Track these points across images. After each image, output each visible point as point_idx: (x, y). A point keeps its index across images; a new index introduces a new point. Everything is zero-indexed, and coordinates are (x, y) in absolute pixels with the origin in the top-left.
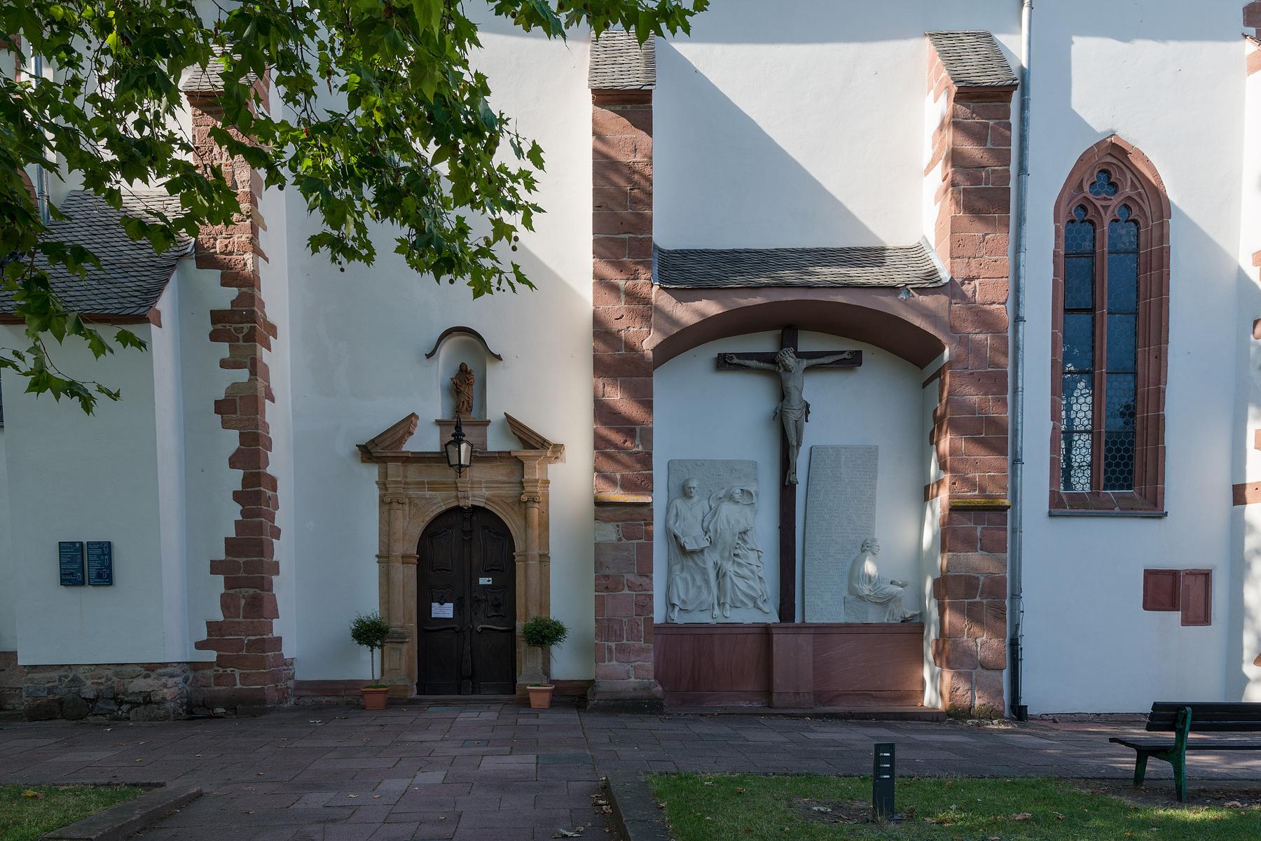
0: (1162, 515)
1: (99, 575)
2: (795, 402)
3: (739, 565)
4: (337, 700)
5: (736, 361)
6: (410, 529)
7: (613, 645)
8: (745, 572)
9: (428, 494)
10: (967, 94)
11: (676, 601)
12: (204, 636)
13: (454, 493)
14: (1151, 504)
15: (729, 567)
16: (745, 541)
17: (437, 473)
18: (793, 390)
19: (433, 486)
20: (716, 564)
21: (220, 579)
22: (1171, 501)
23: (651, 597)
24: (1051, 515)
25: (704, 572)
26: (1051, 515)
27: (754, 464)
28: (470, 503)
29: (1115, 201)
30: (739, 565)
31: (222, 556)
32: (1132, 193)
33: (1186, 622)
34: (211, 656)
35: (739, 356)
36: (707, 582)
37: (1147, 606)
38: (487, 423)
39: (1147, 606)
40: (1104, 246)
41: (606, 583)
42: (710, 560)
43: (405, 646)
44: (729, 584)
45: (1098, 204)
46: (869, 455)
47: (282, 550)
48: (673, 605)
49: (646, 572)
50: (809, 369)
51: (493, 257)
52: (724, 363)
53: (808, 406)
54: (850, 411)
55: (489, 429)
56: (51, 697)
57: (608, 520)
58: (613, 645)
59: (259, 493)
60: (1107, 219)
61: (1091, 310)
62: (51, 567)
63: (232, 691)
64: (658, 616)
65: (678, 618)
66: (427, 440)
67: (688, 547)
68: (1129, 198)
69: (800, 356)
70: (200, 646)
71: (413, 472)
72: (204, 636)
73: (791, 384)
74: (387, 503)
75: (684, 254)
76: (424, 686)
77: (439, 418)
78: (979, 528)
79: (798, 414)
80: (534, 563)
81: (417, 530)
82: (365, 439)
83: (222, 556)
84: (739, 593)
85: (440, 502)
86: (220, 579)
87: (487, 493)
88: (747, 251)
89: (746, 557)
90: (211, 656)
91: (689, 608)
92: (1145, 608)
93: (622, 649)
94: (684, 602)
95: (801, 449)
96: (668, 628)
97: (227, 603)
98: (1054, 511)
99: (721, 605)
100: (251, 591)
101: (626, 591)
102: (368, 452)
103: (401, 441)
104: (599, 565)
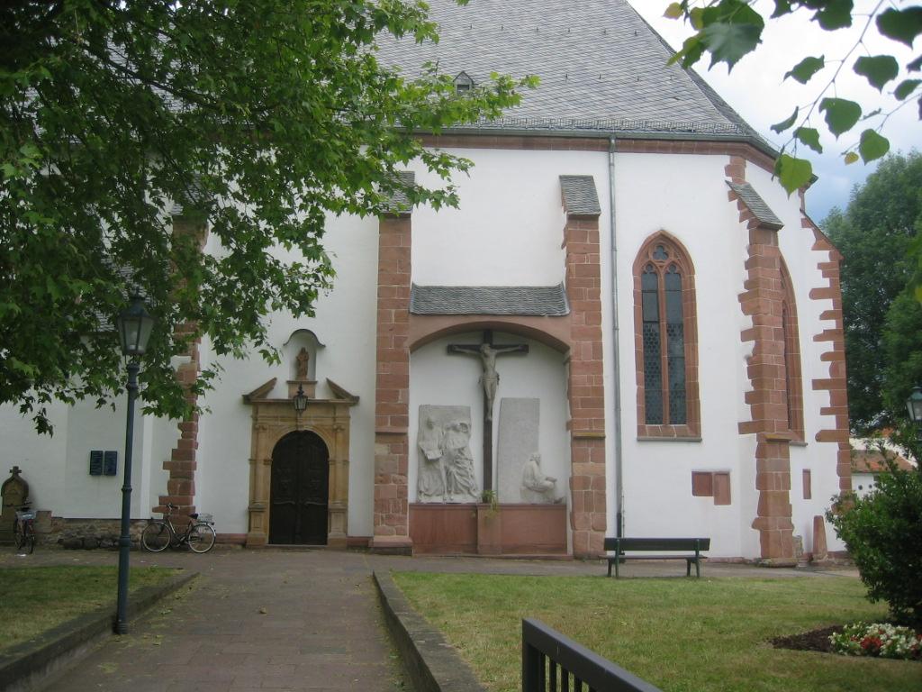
0: (699, 441)
1: (110, 470)
2: (491, 373)
3: (459, 468)
4: (223, 543)
5: (458, 349)
6: (268, 444)
7: (384, 515)
8: (462, 472)
9: (280, 423)
10: (573, 218)
11: (423, 490)
12: (157, 505)
13: (294, 423)
14: (694, 436)
15: (453, 470)
16: (462, 454)
17: (284, 412)
18: (489, 368)
19: (283, 419)
20: (445, 467)
21: (168, 472)
22: (704, 434)
23: (406, 487)
24: (639, 440)
25: (439, 471)
26: (639, 440)
27: (469, 409)
28: (303, 429)
29: (667, 262)
30: (459, 468)
31: (169, 459)
32: (676, 260)
33: (717, 502)
34: (160, 516)
35: (459, 346)
36: (440, 477)
37: (695, 493)
38: (315, 383)
39: (695, 493)
40: (662, 288)
41: (381, 478)
42: (442, 464)
43: (263, 514)
44: (453, 481)
45: (658, 264)
46: (535, 403)
47: (200, 455)
48: (421, 492)
49: (404, 473)
50: (498, 356)
51: (313, 252)
52: (451, 350)
53: (498, 376)
54: (519, 381)
55: (317, 385)
56: (78, 537)
57: (381, 442)
58: (384, 515)
59: (192, 424)
60: (662, 272)
61: (658, 322)
62: (85, 465)
63: (177, 529)
64: (411, 498)
65: (424, 500)
66: (282, 392)
67: (429, 457)
68: (673, 262)
69: (493, 347)
70: (155, 510)
71: (272, 412)
72: (157, 505)
73: (488, 363)
74: (257, 430)
75: (429, 289)
76: (272, 541)
77: (288, 379)
78: (590, 449)
79: (492, 380)
80: (339, 465)
81: (272, 445)
82: (247, 393)
83: (169, 459)
84: (459, 486)
85: (286, 428)
86: (168, 472)
87: (313, 423)
88: (465, 288)
89: (463, 463)
90: (160, 516)
91: (430, 493)
92: (694, 494)
93: (389, 517)
94: (427, 490)
95: (495, 400)
96: (418, 507)
97: (171, 486)
98: (641, 437)
99: (449, 492)
100: (185, 480)
101: (392, 484)
102: (247, 399)
103: (266, 393)
104: (377, 467)
